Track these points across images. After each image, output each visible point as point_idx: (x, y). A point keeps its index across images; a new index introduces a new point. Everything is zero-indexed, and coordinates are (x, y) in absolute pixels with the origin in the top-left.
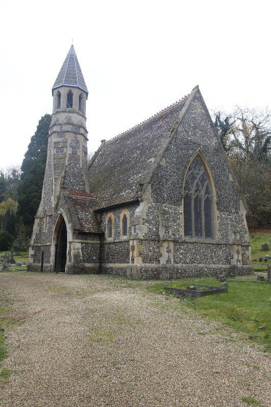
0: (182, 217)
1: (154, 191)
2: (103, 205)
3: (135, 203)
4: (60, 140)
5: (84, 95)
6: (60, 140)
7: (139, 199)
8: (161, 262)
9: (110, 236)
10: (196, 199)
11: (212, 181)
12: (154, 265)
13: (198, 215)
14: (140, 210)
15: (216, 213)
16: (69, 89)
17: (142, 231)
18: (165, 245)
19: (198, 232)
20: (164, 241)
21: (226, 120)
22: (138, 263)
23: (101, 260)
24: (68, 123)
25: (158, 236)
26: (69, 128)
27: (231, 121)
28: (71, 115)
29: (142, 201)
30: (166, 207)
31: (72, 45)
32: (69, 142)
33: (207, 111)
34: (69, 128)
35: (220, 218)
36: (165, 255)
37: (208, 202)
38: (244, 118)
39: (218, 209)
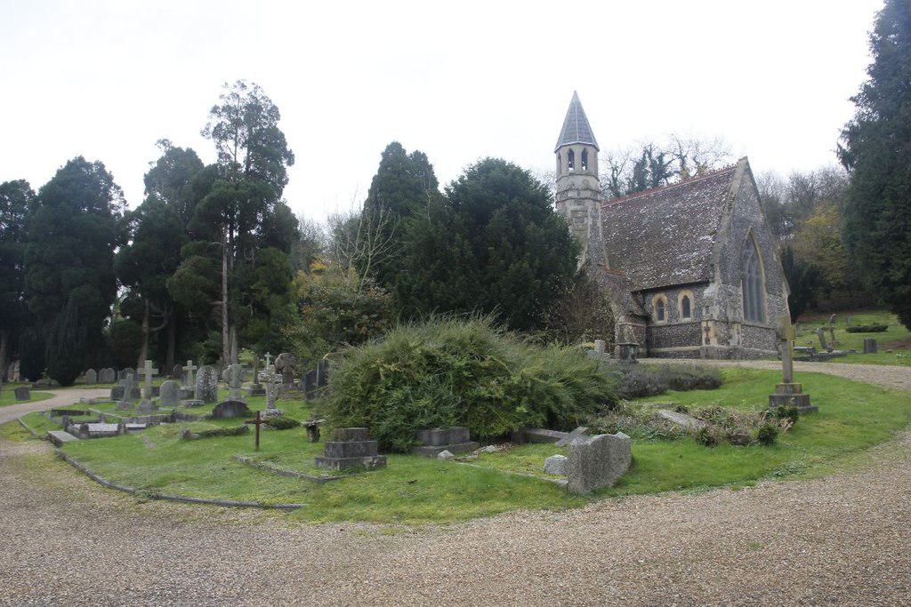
0: (742, 299)
1: (722, 271)
2: (646, 285)
3: (705, 283)
4: (579, 208)
5: (590, 151)
6: (579, 208)
7: (710, 280)
8: (731, 344)
9: (661, 317)
10: (750, 280)
11: (761, 261)
12: (725, 347)
13: (751, 300)
14: (709, 292)
15: (766, 296)
16: (568, 147)
17: (716, 312)
18: (735, 326)
19: (753, 318)
20: (734, 323)
21: (660, 158)
22: (714, 343)
23: (648, 343)
24: (587, 189)
25: (727, 318)
26: (588, 194)
27: (666, 159)
28: (589, 178)
29: (713, 282)
30: (731, 288)
31: (575, 92)
32: (590, 210)
33: (754, 184)
34: (588, 194)
35: (769, 301)
36: (736, 337)
37: (758, 282)
38: (684, 154)
39: (767, 291)
